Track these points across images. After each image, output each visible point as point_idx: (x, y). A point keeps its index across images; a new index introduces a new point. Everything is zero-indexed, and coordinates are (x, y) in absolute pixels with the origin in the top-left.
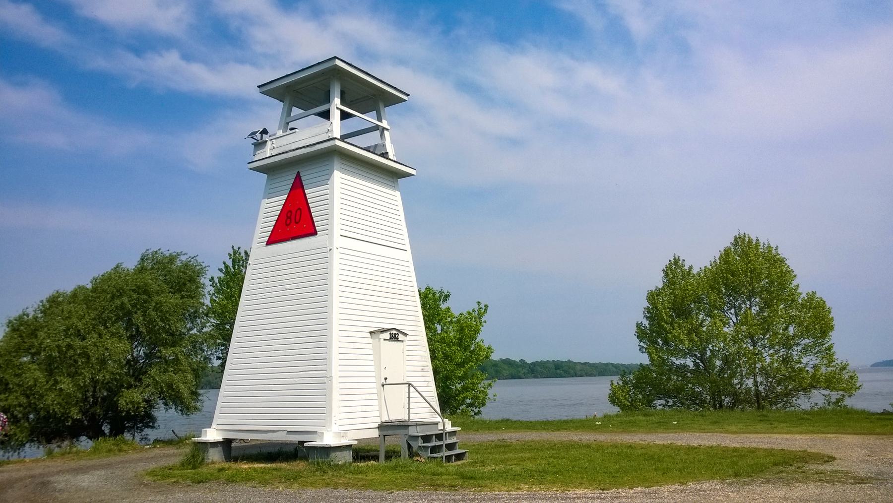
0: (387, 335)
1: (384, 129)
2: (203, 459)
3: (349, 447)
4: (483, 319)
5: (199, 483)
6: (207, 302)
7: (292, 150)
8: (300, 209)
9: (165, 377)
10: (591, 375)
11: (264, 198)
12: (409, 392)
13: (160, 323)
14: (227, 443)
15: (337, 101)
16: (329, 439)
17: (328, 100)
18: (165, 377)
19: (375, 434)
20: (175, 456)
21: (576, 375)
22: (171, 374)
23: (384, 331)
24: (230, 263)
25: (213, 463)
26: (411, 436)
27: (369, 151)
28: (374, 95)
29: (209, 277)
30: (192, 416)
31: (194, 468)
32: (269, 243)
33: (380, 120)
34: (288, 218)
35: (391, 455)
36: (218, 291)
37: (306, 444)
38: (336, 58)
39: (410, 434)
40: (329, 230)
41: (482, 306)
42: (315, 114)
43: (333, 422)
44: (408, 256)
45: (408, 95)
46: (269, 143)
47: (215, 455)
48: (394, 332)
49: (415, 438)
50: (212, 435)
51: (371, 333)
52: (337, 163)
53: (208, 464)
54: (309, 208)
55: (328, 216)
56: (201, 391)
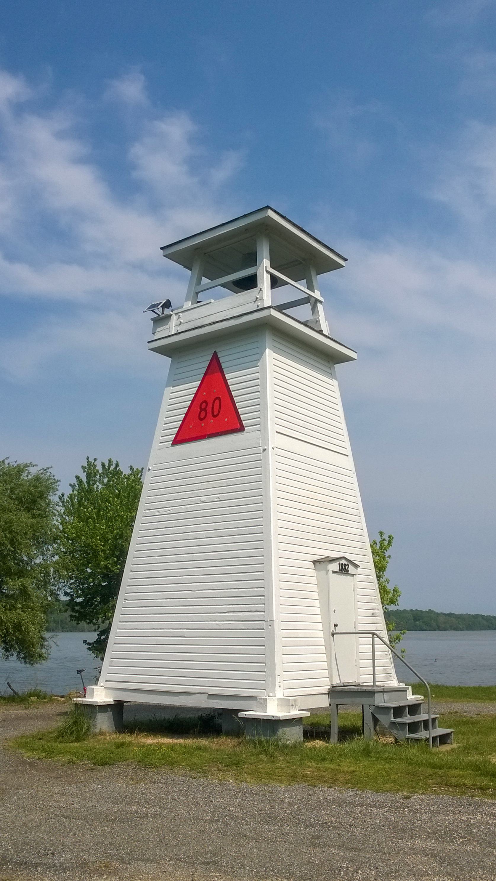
0: (335, 566)
1: (317, 301)
2: (88, 729)
3: (298, 721)
4: (387, 554)
5: (104, 764)
6: (56, 521)
7: (210, 324)
8: (219, 398)
9: (13, 615)
10: (456, 629)
11: (167, 386)
12: (373, 645)
13: (9, 547)
14: (118, 707)
15: (266, 262)
16: (273, 710)
17: (252, 260)
18: (13, 615)
19: (324, 702)
20: (46, 720)
21: (438, 628)
22: (19, 611)
23: (332, 560)
24: (83, 477)
25: (102, 733)
26: (379, 708)
27: (306, 325)
28: (304, 260)
29: (59, 493)
30: (36, 666)
31: (78, 740)
32: (176, 442)
33: (310, 287)
34: (202, 410)
35: (347, 733)
36: (69, 513)
37: (241, 715)
38: (268, 207)
39: (377, 704)
40: (261, 426)
41: (385, 537)
42: (224, 285)
43: (277, 684)
44: (349, 463)
45: (345, 260)
46: (174, 318)
47: (104, 723)
48: (344, 562)
49: (384, 710)
50: (100, 695)
51: (314, 562)
52: (268, 339)
53: (95, 735)
54: (232, 398)
55: (260, 406)
56: (47, 635)
